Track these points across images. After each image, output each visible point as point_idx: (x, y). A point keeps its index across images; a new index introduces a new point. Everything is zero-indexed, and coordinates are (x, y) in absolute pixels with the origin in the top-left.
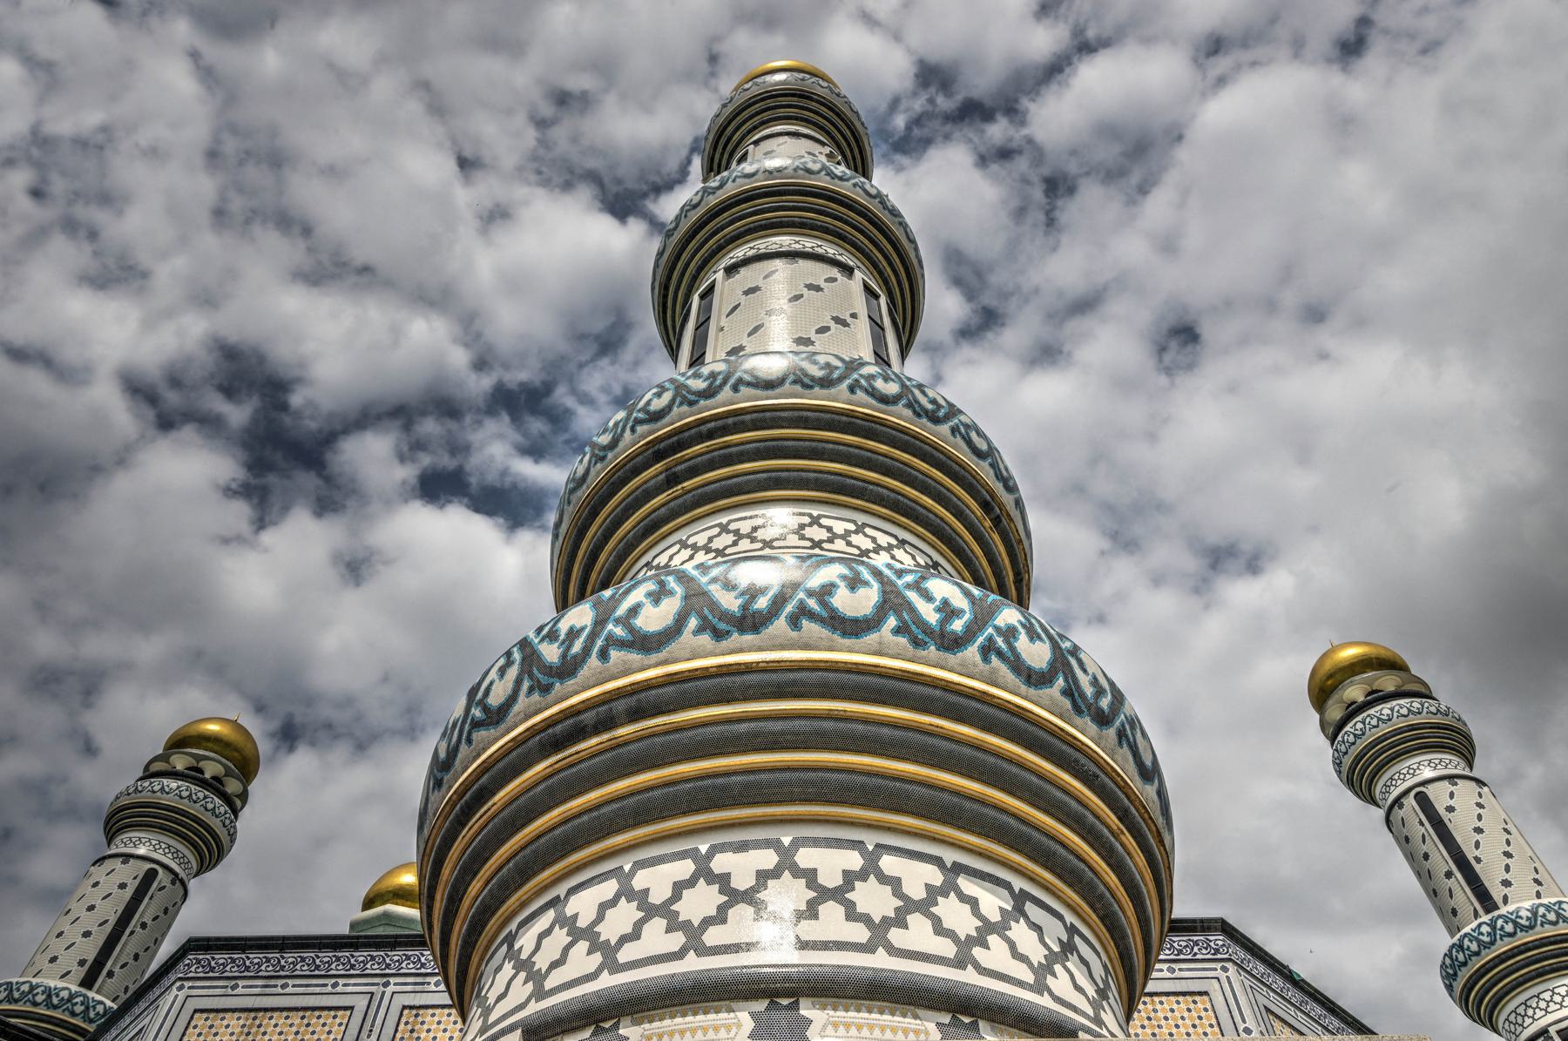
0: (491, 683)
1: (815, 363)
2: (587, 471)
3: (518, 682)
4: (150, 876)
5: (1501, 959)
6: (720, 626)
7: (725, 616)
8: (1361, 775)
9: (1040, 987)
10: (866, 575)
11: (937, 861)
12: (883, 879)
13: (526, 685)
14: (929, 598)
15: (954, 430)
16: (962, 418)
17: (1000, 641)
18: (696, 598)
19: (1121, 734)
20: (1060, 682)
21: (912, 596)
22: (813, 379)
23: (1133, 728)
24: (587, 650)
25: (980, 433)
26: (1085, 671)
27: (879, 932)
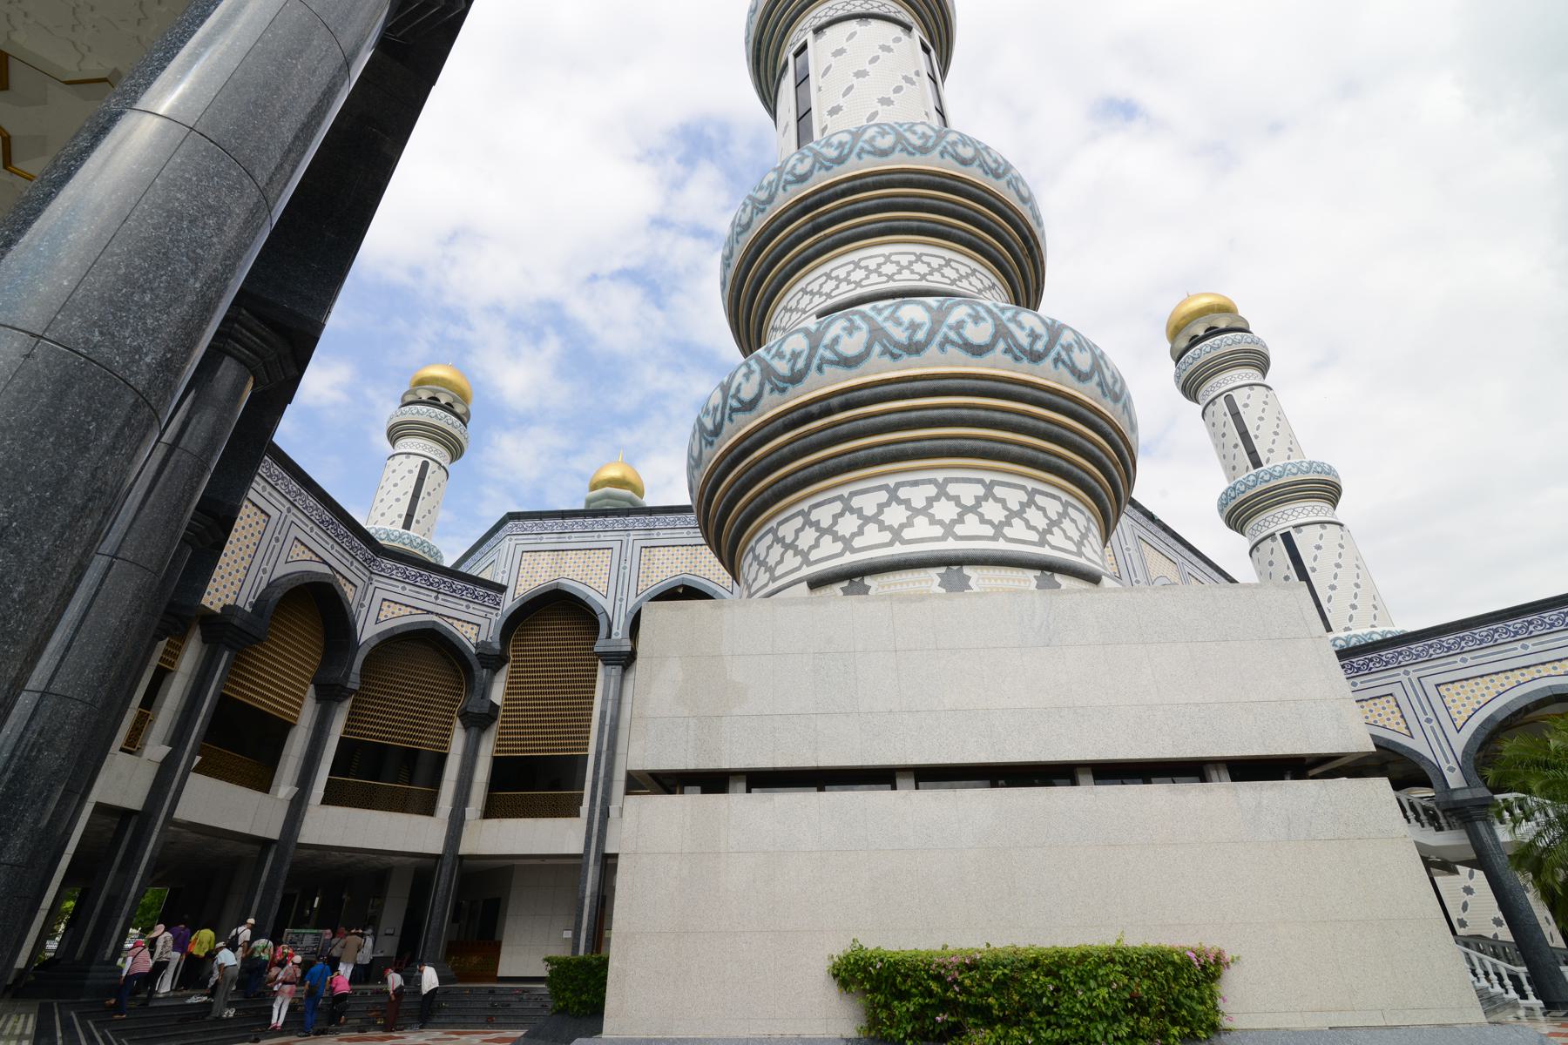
1: (914, 133)
2: (751, 220)
3: (762, 386)
4: (425, 466)
5: (1257, 495)
6: (895, 351)
7: (897, 344)
8: (1190, 388)
9: (1080, 554)
10: (983, 313)
11: (1023, 488)
12: (997, 500)
14: (1021, 326)
18: (876, 333)
22: (914, 147)
24: (808, 366)
27: (999, 528)
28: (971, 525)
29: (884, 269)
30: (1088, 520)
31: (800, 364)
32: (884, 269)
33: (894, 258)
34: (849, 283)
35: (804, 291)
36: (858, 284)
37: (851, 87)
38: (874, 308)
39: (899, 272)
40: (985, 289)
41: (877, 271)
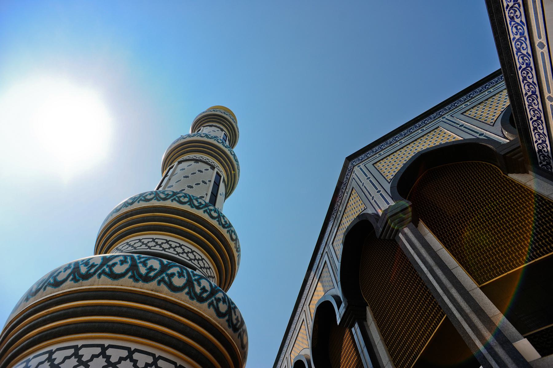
0: (60, 272)
1: (197, 201)
7: (195, 294)
13: (71, 277)
14: (199, 284)
16: (232, 229)
17: (215, 302)
20: (227, 317)
21: (195, 283)
23: (244, 333)
25: (235, 234)
26: (235, 314)
29: (164, 246)
31: (205, 295)
32: (177, 249)
33: (183, 247)
34: (161, 247)
36: (164, 249)
37: (184, 177)
39: (182, 253)
41: (174, 248)
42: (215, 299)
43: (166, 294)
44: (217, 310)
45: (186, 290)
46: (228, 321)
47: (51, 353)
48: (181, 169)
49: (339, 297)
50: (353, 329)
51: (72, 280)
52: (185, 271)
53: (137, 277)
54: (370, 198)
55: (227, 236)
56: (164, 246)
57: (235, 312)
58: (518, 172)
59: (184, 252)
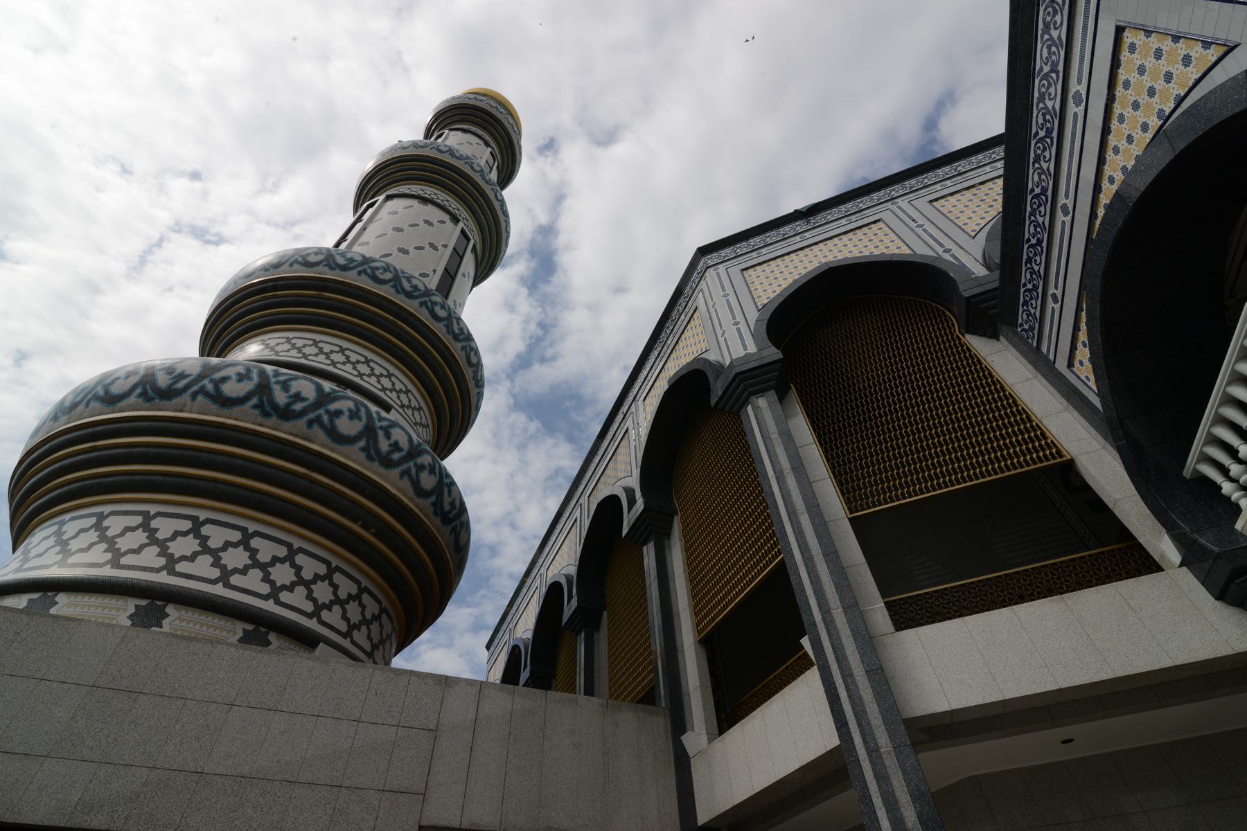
7: (378, 452)
15: (464, 348)
17: (414, 471)
19: (454, 529)
20: (433, 498)
26: (450, 495)
28: (297, 598)
29: (334, 356)
30: (394, 629)
31: (396, 456)
33: (372, 364)
34: (328, 358)
35: (288, 340)
36: (334, 364)
37: (394, 229)
38: (378, 413)
39: (369, 376)
40: (421, 424)
41: (354, 364)
42: (415, 464)
43: (322, 445)
44: (416, 484)
45: (362, 443)
46: (433, 504)
47: (101, 517)
48: (393, 212)
49: (633, 491)
50: (645, 549)
51: (140, 395)
52: (363, 409)
53: (268, 408)
54: (719, 332)
55: (460, 357)
56: (334, 356)
57: (450, 492)
58: (983, 334)
59: (374, 374)
